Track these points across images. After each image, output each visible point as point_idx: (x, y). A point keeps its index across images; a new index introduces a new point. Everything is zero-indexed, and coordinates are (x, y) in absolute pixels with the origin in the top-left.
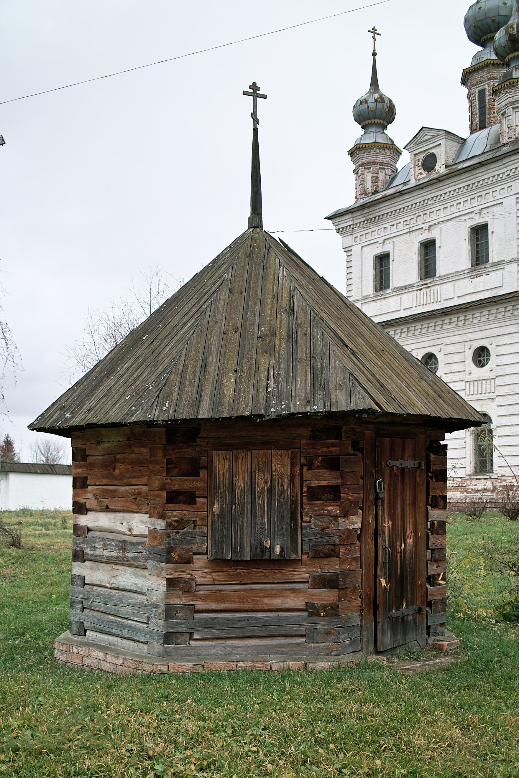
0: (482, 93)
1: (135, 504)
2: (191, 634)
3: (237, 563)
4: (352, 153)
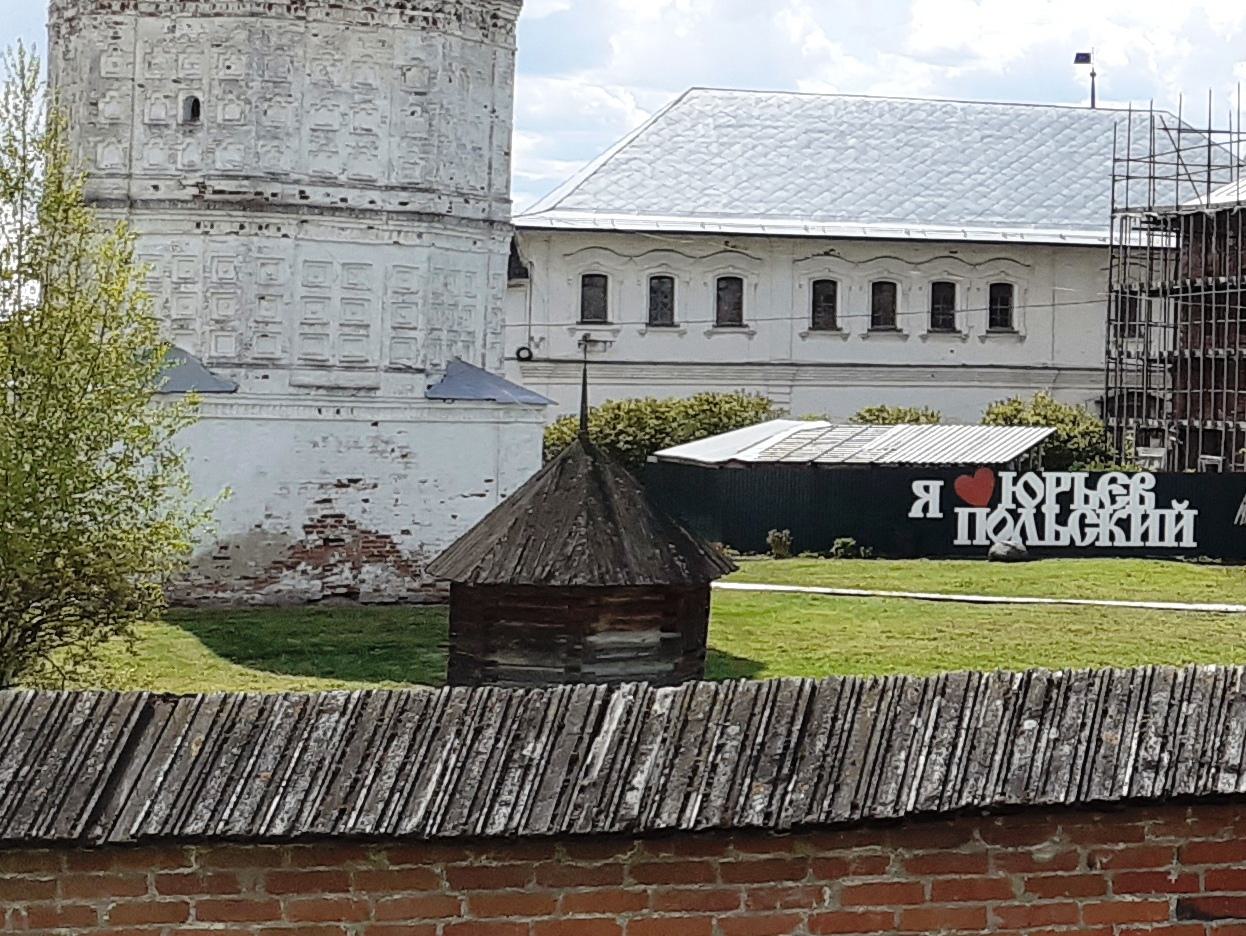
1: (647, 626)
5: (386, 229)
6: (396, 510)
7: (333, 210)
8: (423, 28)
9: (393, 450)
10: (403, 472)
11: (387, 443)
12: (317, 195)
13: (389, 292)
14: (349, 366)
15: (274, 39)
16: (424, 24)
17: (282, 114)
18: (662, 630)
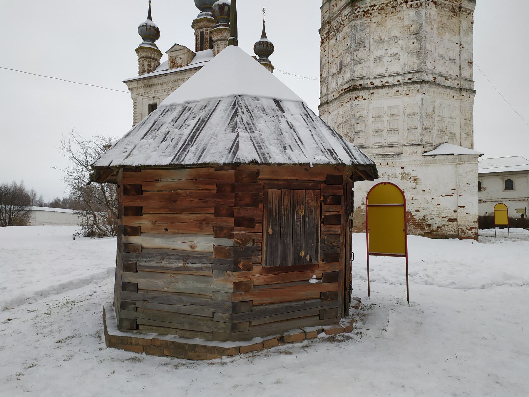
0: (202, 33)
1: (199, 227)
2: (250, 323)
3: (283, 269)
4: (137, 50)
5: (403, 89)
6: (413, 202)
7: (382, 87)
8: (415, 8)
9: (410, 178)
10: (414, 186)
11: (408, 175)
12: (377, 82)
13: (406, 115)
14: (392, 146)
15: (358, 28)
16: (416, 6)
17: (362, 53)
18: (217, 235)
